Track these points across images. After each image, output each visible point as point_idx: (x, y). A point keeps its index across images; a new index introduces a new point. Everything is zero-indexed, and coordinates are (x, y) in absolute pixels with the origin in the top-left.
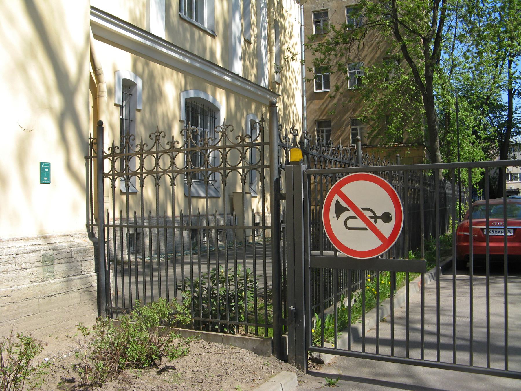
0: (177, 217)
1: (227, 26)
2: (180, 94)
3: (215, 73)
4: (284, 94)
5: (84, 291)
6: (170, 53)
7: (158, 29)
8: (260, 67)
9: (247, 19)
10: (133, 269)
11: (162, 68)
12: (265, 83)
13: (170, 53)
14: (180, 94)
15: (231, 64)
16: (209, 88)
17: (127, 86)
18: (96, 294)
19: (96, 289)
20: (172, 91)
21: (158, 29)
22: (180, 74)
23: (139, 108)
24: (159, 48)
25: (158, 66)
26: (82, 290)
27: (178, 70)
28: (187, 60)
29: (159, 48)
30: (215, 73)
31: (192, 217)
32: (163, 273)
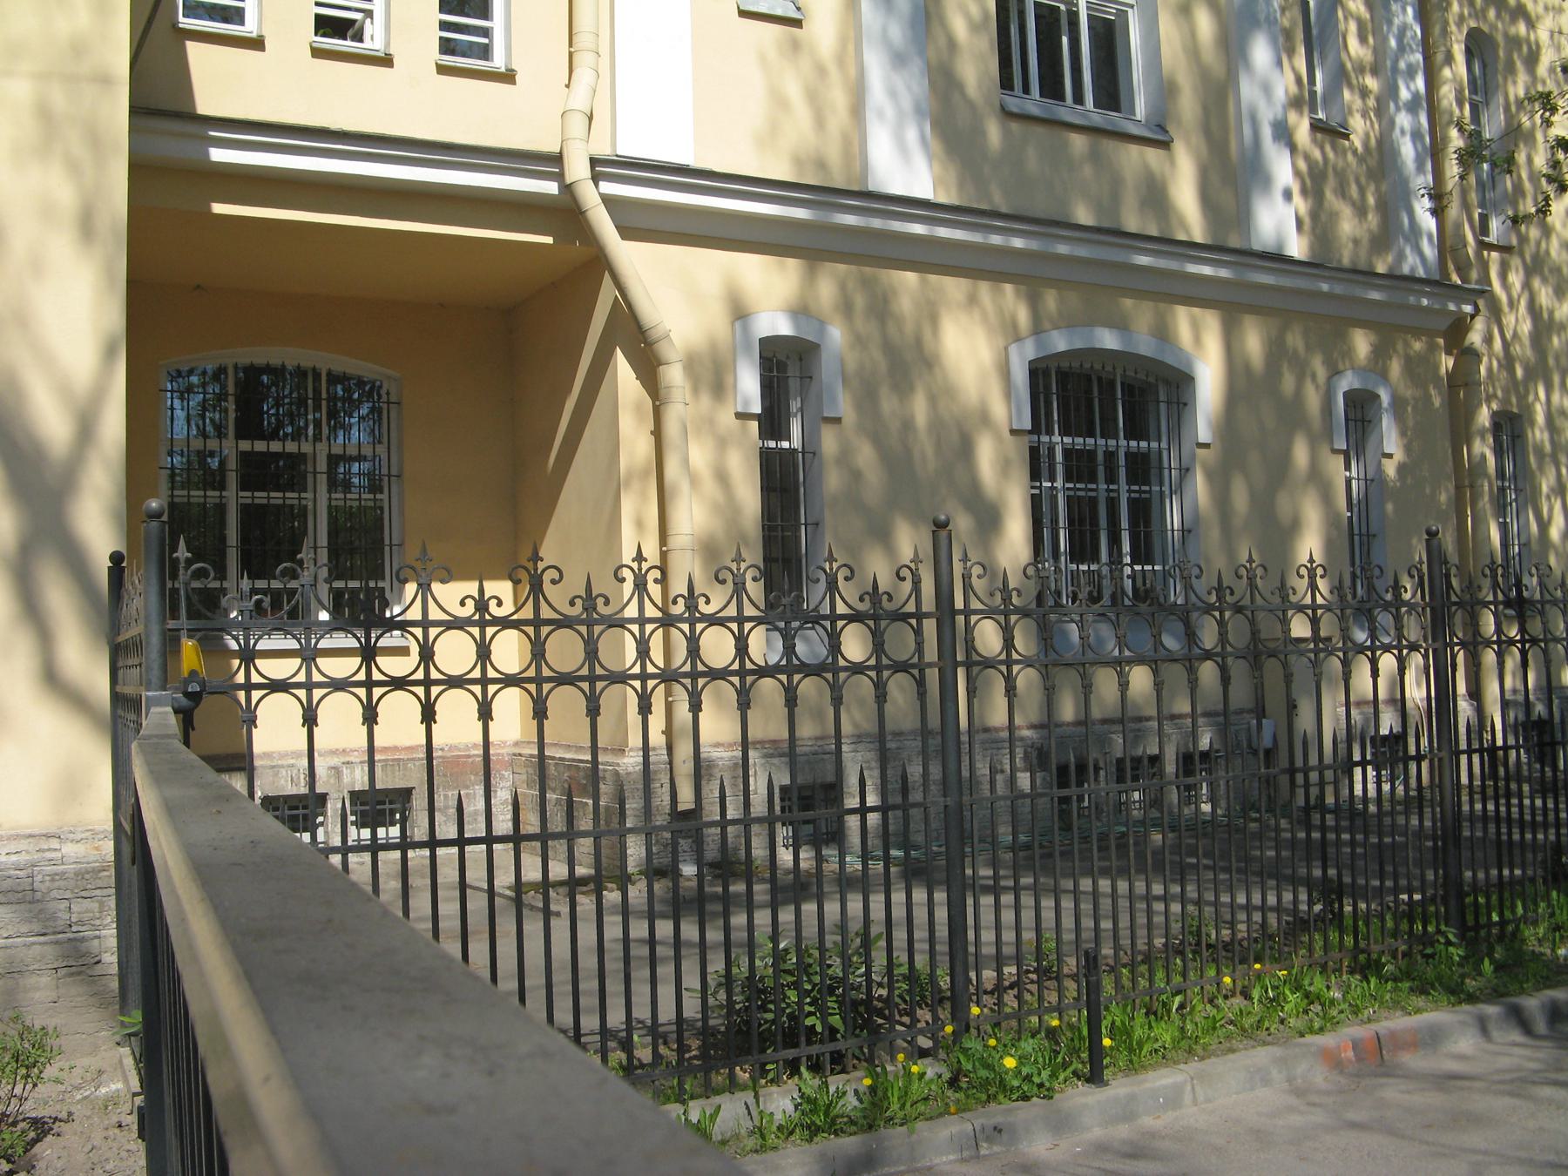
0: (1020, 728)
1: (1219, 93)
2: (1006, 348)
3: (1143, 260)
4: (1536, 283)
5: (65, 976)
6: (943, 232)
7: (904, 166)
8: (1393, 204)
9: (1330, 59)
10: (737, 895)
11: (924, 282)
12: (1420, 257)
13: (943, 232)
14: (1006, 348)
15: (1243, 218)
16: (1142, 315)
17: (786, 366)
18: (115, 985)
19: (115, 969)
20: (976, 351)
21: (904, 166)
22: (1008, 288)
23: (1387, 451)
24: (897, 226)
25: (911, 277)
26: (62, 972)
27: (996, 276)
28: (1018, 243)
29: (897, 226)
30: (1143, 260)
31: (1097, 727)
32: (877, 901)
